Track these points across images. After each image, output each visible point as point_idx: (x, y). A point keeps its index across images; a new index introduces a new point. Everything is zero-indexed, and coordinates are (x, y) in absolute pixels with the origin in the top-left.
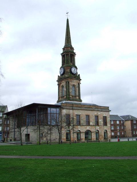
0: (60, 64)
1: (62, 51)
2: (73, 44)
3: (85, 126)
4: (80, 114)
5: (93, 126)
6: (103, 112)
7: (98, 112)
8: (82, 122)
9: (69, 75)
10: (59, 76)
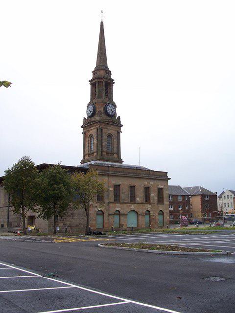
0: (87, 99)
1: (91, 77)
2: (111, 65)
3: (128, 204)
4: (120, 183)
5: (142, 203)
6: (158, 181)
7: (149, 181)
8: (123, 196)
9: (102, 122)
10: (85, 118)
